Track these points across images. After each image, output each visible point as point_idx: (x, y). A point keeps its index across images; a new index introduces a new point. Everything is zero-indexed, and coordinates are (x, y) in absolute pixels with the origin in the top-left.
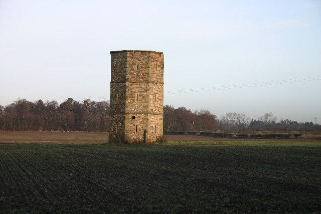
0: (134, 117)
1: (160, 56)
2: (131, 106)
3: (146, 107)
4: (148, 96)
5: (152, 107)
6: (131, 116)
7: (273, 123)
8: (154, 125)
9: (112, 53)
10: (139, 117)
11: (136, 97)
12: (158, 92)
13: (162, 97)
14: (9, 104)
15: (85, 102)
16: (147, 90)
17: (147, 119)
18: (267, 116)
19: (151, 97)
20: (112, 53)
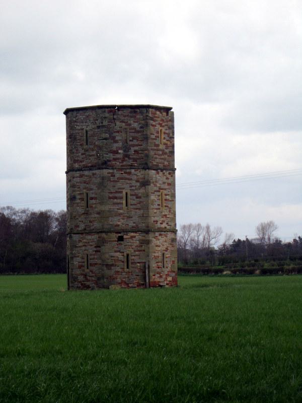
0: (121, 239)
1: (167, 115)
2: (144, 230)
3: (145, 217)
4: (147, 196)
5: (156, 219)
6: (114, 236)
7: (278, 243)
8: (160, 254)
9: (67, 112)
10: (132, 237)
11: (125, 198)
12: (166, 186)
13: (174, 196)
14: (38, 276)
15: (295, 240)
16: (145, 183)
17: (148, 242)
18: (264, 229)
19: (153, 197)
20: (67, 112)
